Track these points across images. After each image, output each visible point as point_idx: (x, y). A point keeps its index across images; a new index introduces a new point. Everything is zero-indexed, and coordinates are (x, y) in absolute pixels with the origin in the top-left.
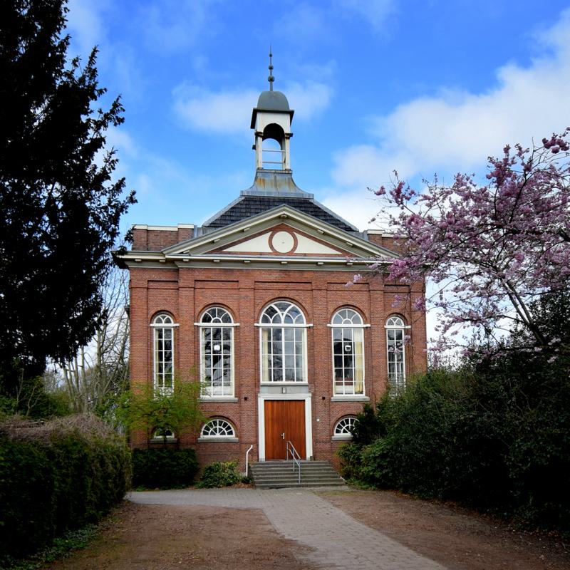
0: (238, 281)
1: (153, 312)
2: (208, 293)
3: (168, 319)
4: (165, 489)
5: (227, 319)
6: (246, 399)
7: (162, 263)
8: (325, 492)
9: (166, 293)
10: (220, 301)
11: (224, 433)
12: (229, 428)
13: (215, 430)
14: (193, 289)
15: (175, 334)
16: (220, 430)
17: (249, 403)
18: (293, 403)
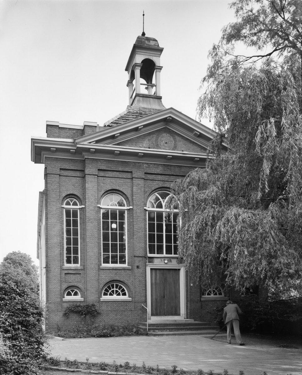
0: (131, 172)
1: (64, 195)
2: (108, 180)
3: (75, 201)
4: (240, 330)
5: (75, 204)
6: (138, 267)
7: (72, 153)
8: (223, 336)
9: (74, 180)
10: (117, 188)
11: (119, 295)
12: (123, 290)
13: (113, 291)
14: (96, 176)
15: (80, 214)
16: (117, 291)
17: (141, 270)
18: (171, 272)
